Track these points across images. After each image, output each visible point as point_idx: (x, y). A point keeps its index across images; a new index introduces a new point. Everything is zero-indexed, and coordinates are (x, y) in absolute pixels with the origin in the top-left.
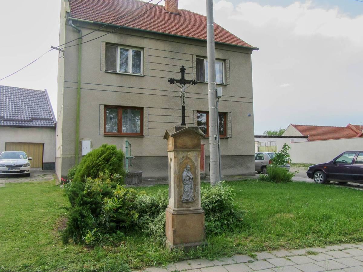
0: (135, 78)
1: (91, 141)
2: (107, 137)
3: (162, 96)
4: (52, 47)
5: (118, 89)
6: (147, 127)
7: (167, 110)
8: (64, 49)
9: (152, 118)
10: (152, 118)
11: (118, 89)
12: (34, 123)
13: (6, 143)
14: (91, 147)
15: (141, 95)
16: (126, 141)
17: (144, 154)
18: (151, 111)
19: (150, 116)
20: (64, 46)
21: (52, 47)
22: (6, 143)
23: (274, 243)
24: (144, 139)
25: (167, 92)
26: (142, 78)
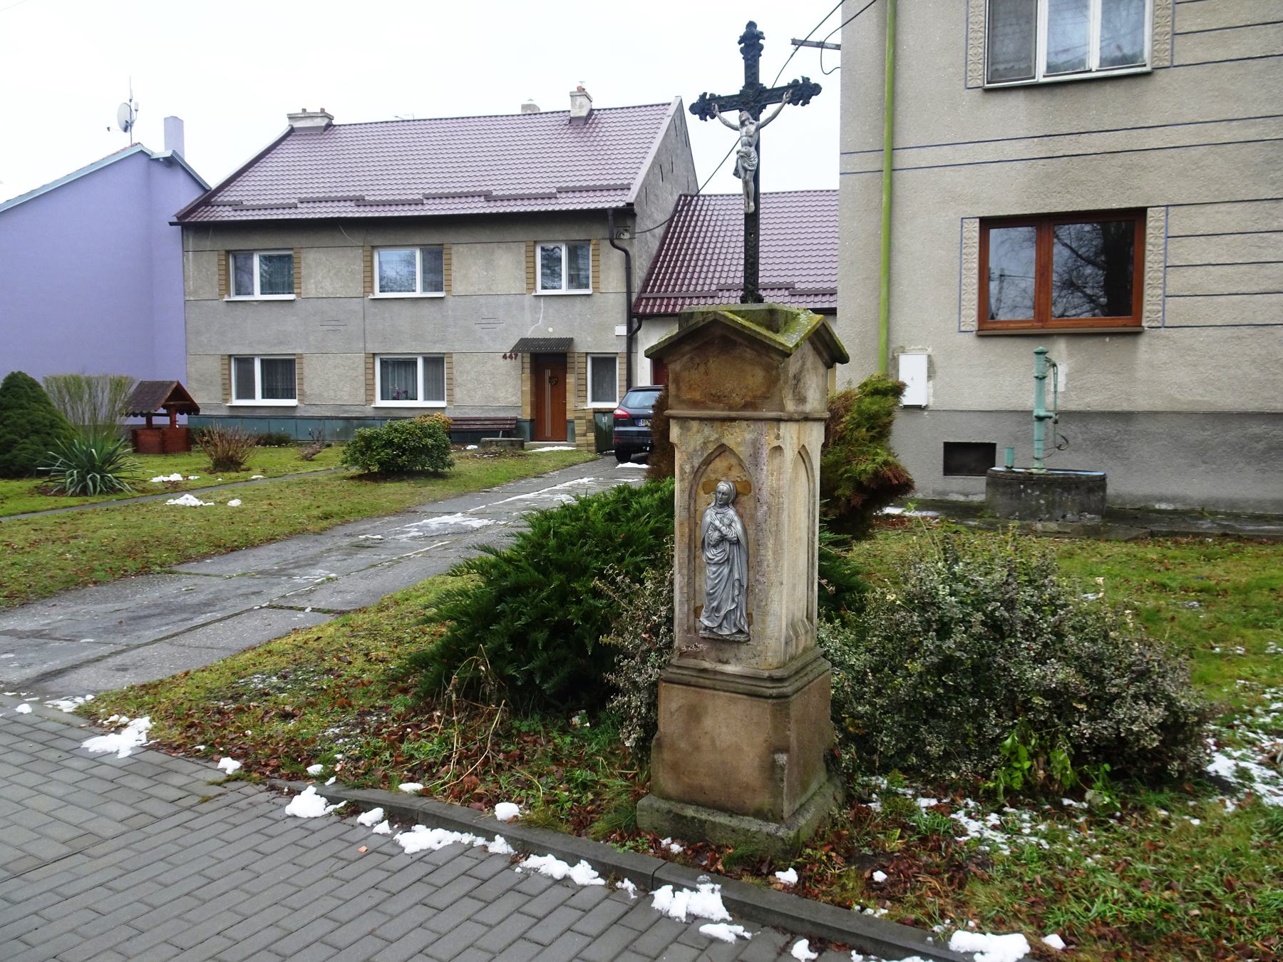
0: (1108, 89)
1: (929, 356)
2: (986, 340)
3: (1243, 144)
4: (794, 42)
5: (1037, 149)
6: (1160, 292)
7: (1267, 204)
8: (836, 39)
9: (1184, 252)
10: (1184, 252)
11: (1037, 149)
12: (725, 301)
13: (949, 448)
14: (929, 377)
15: (1134, 156)
16: (1038, 353)
17: (1142, 403)
18: (1181, 222)
19: (1173, 244)
20: (837, 19)
21: (794, 42)
22: (949, 448)
23: (1168, 569)
24: (1143, 341)
25: (1269, 120)
26: (1143, 82)
